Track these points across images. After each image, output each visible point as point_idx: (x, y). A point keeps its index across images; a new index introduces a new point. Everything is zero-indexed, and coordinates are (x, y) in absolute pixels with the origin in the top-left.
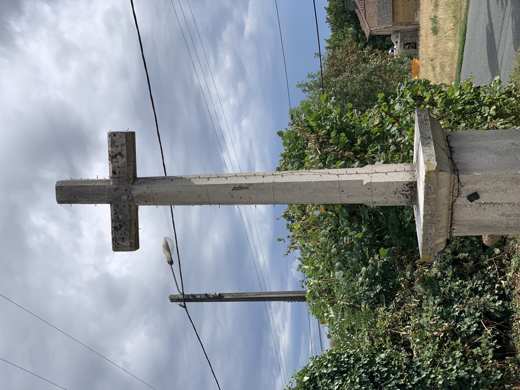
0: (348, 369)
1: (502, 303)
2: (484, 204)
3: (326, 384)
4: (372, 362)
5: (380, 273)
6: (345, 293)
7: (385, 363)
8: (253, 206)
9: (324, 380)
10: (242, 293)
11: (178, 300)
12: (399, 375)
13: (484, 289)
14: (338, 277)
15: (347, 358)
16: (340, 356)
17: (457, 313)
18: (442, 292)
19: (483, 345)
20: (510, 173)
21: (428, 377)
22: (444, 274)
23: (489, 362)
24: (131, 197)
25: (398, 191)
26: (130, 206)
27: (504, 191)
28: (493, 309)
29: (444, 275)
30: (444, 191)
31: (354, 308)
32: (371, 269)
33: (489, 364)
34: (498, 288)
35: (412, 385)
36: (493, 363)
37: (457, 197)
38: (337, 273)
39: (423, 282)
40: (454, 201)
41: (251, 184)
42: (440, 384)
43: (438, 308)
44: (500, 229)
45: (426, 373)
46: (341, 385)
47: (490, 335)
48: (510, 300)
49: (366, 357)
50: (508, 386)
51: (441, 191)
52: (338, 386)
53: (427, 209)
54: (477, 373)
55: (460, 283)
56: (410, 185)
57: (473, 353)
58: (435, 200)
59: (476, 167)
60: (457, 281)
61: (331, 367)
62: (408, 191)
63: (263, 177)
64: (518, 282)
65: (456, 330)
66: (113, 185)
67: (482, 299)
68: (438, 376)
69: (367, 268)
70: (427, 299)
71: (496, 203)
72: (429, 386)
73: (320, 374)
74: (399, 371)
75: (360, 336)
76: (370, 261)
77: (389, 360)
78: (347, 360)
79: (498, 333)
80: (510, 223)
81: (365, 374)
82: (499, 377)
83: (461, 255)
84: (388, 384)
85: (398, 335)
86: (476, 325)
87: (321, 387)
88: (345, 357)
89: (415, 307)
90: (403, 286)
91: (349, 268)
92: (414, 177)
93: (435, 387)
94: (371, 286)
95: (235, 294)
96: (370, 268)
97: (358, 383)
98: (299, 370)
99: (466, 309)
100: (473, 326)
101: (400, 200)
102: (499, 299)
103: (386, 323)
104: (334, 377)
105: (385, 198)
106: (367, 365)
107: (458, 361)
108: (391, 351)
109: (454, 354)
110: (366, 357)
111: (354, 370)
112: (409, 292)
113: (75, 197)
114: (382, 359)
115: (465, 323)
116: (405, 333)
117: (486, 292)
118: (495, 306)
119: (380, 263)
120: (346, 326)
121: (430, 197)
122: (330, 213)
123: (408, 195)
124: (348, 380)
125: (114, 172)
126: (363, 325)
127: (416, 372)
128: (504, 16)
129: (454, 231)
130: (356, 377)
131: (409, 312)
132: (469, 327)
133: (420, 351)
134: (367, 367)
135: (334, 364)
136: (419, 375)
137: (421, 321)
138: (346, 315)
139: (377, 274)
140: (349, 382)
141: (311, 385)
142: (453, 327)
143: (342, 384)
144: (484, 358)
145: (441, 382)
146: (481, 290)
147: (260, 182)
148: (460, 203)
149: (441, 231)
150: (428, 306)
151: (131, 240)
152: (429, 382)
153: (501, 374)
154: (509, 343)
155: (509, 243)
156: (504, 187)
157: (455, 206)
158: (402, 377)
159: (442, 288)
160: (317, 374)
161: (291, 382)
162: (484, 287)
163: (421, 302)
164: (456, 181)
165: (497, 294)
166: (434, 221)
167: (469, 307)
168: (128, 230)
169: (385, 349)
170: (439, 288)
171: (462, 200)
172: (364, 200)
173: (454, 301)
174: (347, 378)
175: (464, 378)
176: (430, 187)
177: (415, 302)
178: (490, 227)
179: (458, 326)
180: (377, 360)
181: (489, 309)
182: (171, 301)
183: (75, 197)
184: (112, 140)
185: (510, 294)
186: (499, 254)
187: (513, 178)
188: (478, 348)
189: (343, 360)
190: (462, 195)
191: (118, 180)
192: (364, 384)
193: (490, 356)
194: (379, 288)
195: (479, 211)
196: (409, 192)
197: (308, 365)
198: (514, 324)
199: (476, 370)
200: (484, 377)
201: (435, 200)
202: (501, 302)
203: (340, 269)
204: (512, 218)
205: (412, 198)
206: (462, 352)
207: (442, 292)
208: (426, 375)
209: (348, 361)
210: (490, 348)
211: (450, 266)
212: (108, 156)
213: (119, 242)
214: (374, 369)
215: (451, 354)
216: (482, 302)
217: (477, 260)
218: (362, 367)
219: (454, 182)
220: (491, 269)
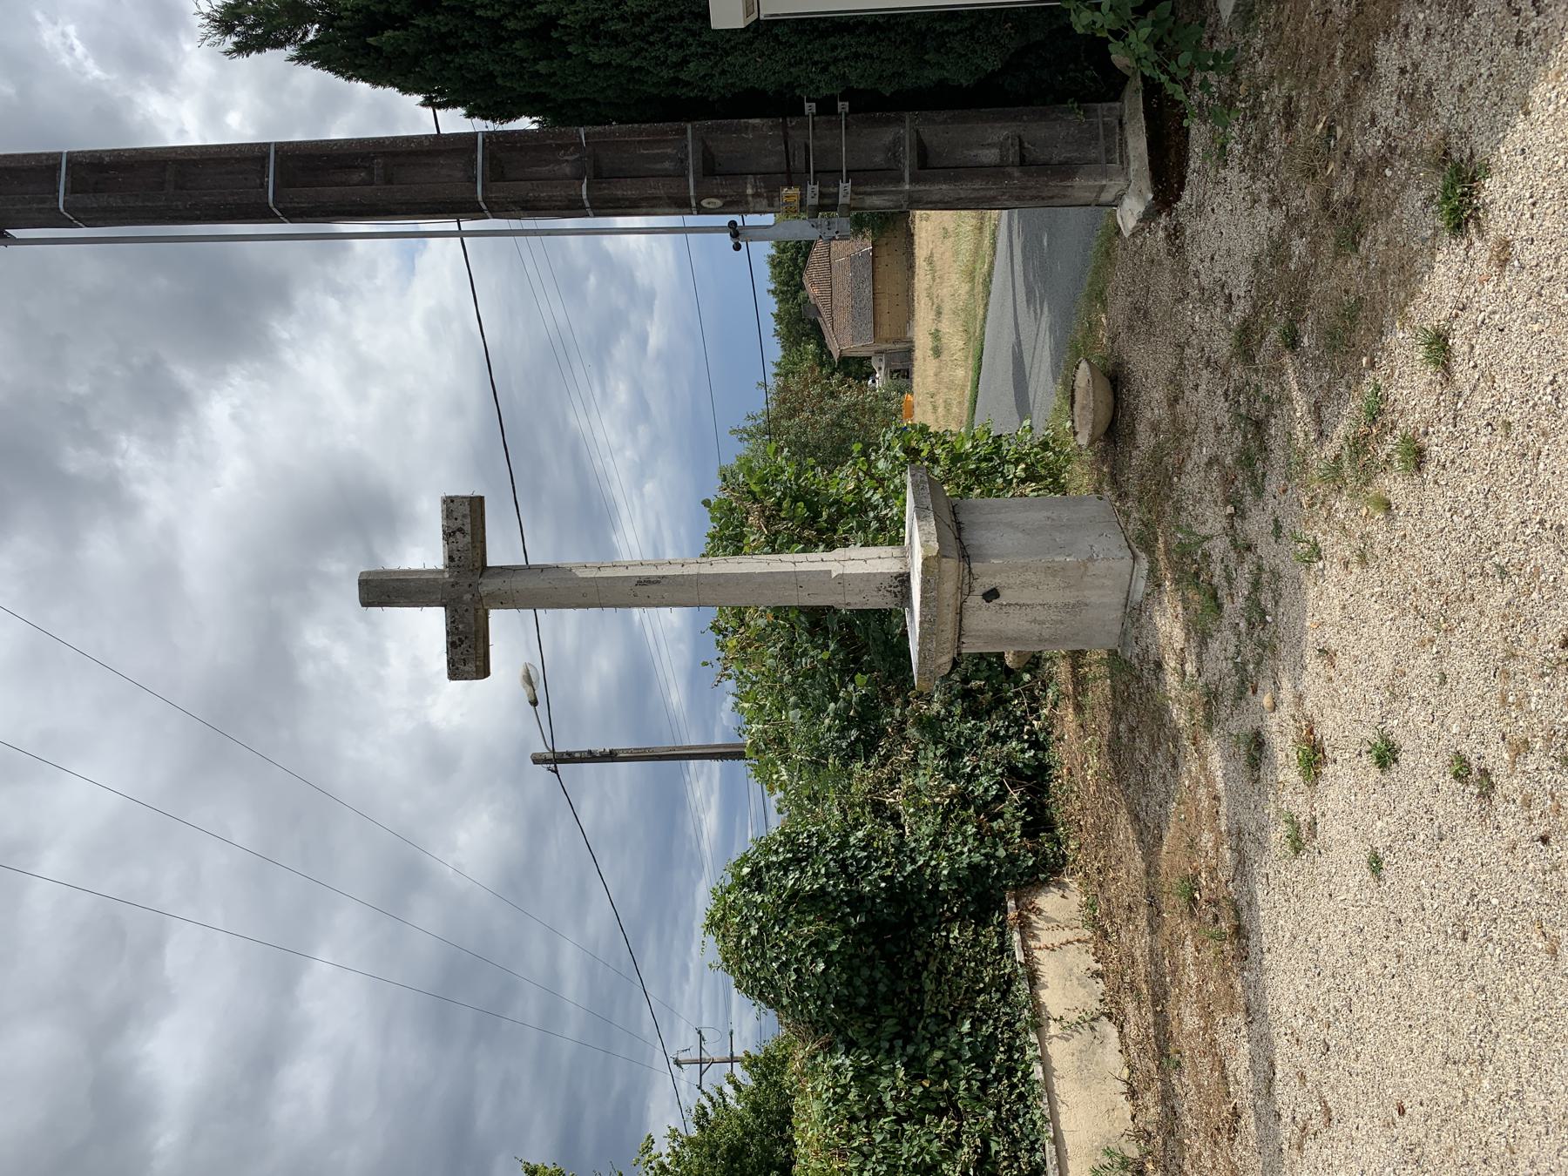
0: (809, 855)
4: (844, 845)
5: (856, 711)
8: (668, 609)
9: (773, 872)
11: (545, 761)
18: (947, 738)
19: (1007, 816)
21: (927, 864)
22: (950, 712)
26: (476, 610)
29: (950, 714)
30: (949, 587)
31: (817, 765)
32: (842, 706)
41: (663, 577)
46: (799, 879)
57: (992, 828)
70: (925, 749)
76: (841, 695)
82: (1030, 863)
83: (974, 684)
89: (907, 761)
94: (843, 731)
96: (841, 704)
98: (736, 857)
102: (1029, 748)
103: (866, 787)
116: (892, 800)
120: (806, 792)
125: (451, 558)
126: (831, 790)
127: (910, 857)
132: (986, 790)
136: (914, 861)
137: (916, 782)
138: (806, 776)
139: (851, 713)
140: (810, 874)
145: (945, 872)
150: (927, 759)
152: (928, 871)
158: (888, 865)
160: (763, 863)
162: (1007, 731)
163: (916, 753)
164: (966, 571)
165: (1026, 741)
167: (987, 760)
170: (942, 732)
171: (975, 600)
173: (964, 751)
177: (907, 754)
178: (1016, 639)
180: (852, 840)
182: (535, 763)
186: (1030, 682)
188: (1000, 820)
190: (975, 593)
193: (1018, 833)
194: (854, 733)
198: (1052, 784)
199: (997, 854)
203: (796, 706)
207: (947, 738)
217: (997, 691)
218: (830, 852)
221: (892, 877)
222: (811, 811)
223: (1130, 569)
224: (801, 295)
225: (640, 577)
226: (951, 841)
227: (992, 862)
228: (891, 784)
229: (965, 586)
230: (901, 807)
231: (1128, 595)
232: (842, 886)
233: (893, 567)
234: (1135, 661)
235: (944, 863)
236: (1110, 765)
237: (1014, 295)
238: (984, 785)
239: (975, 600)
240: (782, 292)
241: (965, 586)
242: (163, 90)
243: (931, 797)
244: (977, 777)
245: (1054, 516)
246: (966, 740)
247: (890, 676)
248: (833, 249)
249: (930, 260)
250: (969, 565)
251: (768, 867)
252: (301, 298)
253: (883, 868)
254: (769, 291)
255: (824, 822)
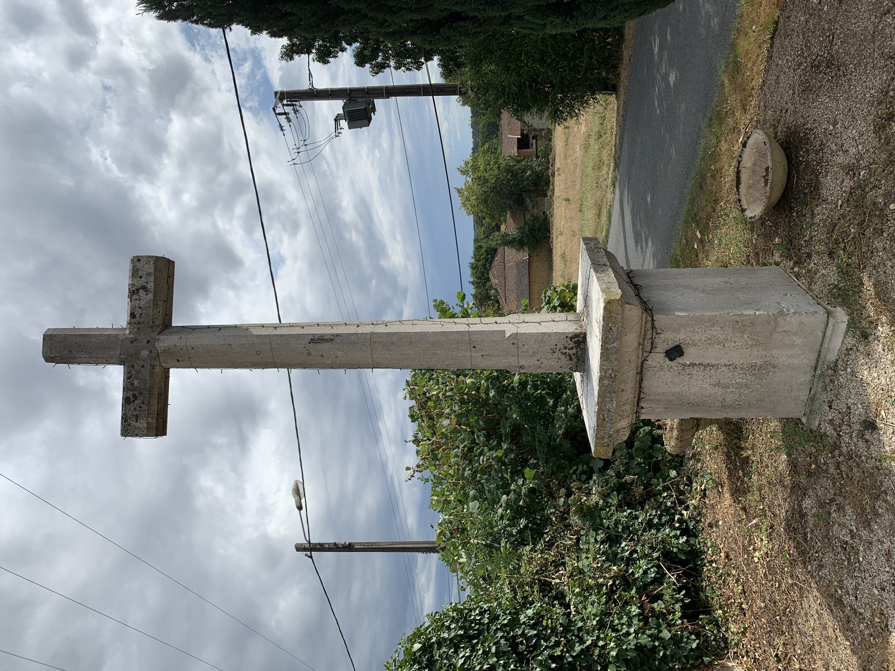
0: (480, 632)
1: (687, 540)
2: (689, 365)
3: (447, 655)
4: (514, 623)
5: (525, 502)
6: (480, 529)
7: (534, 623)
8: (343, 371)
9: (444, 649)
10: (374, 543)
11: (305, 549)
12: (553, 641)
13: (661, 521)
14: (473, 509)
15: (479, 616)
16: (469, 612)
17: (628, 552)
18: (606, 525)
19: (667, 597)
20: (732, 314)
21: (594, 644)
22: (607, 503)
23: (678, 622)
24: (155, 353)
25: (558, 349)
26: (153, 367)
27: (722, 344)
28: (675, 547)
29: (607, 505)
30: (631, 339)
31: (491, 548)
32: (513, 497)
33: (677, 625)
34: (679, 521)
35: (572, 656)
36: (682, 623)
37: (650, 353)
38: (471, 504)
39: (581, 512)
40: (645, 360)
41: (337, 335)
42: (612, 656)
43: (602, 547)
44: (712, 408)
45: (592, 638)
46: (469, 657)
47: (674, 584)
48: (696, 537)
49: (506, 614)
50: (708, 658)
51: (626, 337)
52: (463, 659)
53: (604, 367)
54: (662, 639)
55: (629, 514)
56: (576, 339)
57: (653, 609)
58: (617, 351)
59: (678, 306)
60: (625, 511)
61: (455, 628)
62: (572, 348)
63: (358, 326)
64: (707, 511)
65: (629, 576)
66: (130, 333)
67: (660, 535)
68: (609, 644)
69: (508, 496)
70: (587, 535)
71: (708, 364)
72: (596, 658)
73: (439, 640)
74: (552, 635)
75: (498, 585)
76: (512, 487)
77: (538, 619)
78: (478, 618)
79: (685, 581)
80: (727, 399)
81: (505, 641)
82: (694, 645)
83: (628, 478)
84: (538, 655)
85: (548, 585)
86: (654, 570)
87: (438, 660)
88: (477, 614)
89: (571, 546)
90: (554, 519)
91: (486, 499)
92: (581, 327)
93: (605, 661)
94: (513, 521)
95: (366, 543)
96: (512, 496)
97: (494, 654)
98: (409, 633)
99: (638, 548)
100: (651, 571)
101: (560, 364)
102: (682, 535)
103: (534, 568)
104: (460, 644)
105: (538, 360)
106: (508, 626)
107: (635, 621)
108: (541, 606)
109: (628, 610)
110: (506, 614)
111: (488, 633)
112: (562, 527)
113: (70, 351)
114: (529, 617)
115: (640, 567)
116: (558, 581)
117: (663, 525)
118: (678, 543)
119: (525, 488)
120: (481, 572)
121: (611, 345)
122: (464, 427)
123: (572, 356)
124: (480, 650)
125: (133, 315)
126: (503, 570)
127: (577, 636)
128: (644, 259)
129: (643, 411)
130: (491, 644)
131: (564, 552)
132: (645, 572)
133: (580, 606)
134: (508, 628)
135: (460, 624)
136: (582, 641)
137: (580, 564)
138: (481, 556)
139: (521, 503)
140: (480, 652)
141: (425, 656)
142: (624, 571)
143: (471, 656)
144: (671, 617)
145: (614, 653)
146: (657, 522)
147: (351, 332)
148: (654, 364)
149: (624, 407)
150: (589, 543)
151: (150, 420)
152: (597, 652)
153: (697, 641)
154: (698, 594)
155: (687, 463)
156: (722, 337)
157: (646, 369)
158: (557, 644)
159: (605, 521)
160: (434, 639)
161: (397, 651)
162: (660, 519)
163: (578, 539)
164: (649, 325)
165: (677, 529)
166: (615, 387)
167: (643, 546)
168: (146, 402)
169: (532, 603)
170: (601, 519)
171: (657, 359)
172: (506, 363)
173: (621, 537)
174: (478, 646)
175: (646, 646)
176: (611, 329)
177: (571, 539)
178: (698, 405)
179: (630, 571)
180: (522, 618)
181: (670, 548)
182: (297, 551)
183: (70, 351)
184: (134, 268)
185: (695, 528)
186: (675, 478)
187: (737, 322)
188: (660, 602)
189: (473, 619)
190: (657, 350)
191: (137, 326)
192: (502, 656)
193: (678, 614)
194: (523, 522)
195: (682, 377)
196: (574, 351)
197: (421, 626)
198: (705, 569)
199: (661, 635)
200: (673, 645)
201: (617, 351)
202: (685, 538)
203: (475, 498)
204: (731, 390)
205: (579, 360)
206: (639, 608)
207: (606, 525)
208: (592, 641)
209: (480, 620)
210: (677, 603)
211: (615, 492)
212: (128, 291)
213: (131, 422)
214: (517, 631)
215: (625, 611)
216: (660, 538)
217: (647, 485)
218: (500, 629)
219: (645, 327)
220: (667, 496)
221: (561, 657)
222: (486, 589)
223: (823, 325)
224: (488, 284)
225: (314, 335)
226: (617, 622)
227: (657, 644)
228: (556, 567)
229: (648, 345)
230: (566, 588)
231: (819, 356)
232: (512, 667)
233: (570, 328)
234: (829, 430)
235: (612, 644)
236: (790, 547)
237: (625, 242)
238: (641, 569)
239: (657, 359)
240: (477, 283)
241: (648, 345)
242: (151, 183)
243: (594, 578)
244: (634, 560)
245: (732, 280)
246: (623, 527)
247: (553, 473)
248: (506, 259)
249: (563, 256)
250: (652, 317)
251: (440, 644)
252: (214, 290)
253: (553, 647)
254: (470, 282)
255: (496, 600)
